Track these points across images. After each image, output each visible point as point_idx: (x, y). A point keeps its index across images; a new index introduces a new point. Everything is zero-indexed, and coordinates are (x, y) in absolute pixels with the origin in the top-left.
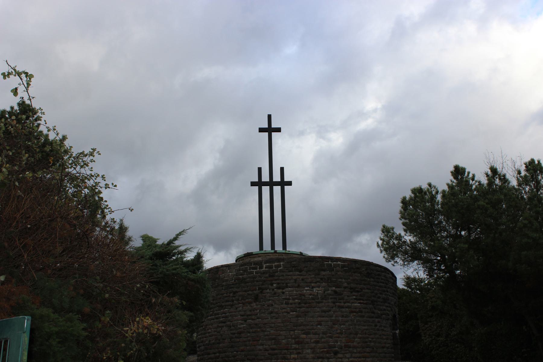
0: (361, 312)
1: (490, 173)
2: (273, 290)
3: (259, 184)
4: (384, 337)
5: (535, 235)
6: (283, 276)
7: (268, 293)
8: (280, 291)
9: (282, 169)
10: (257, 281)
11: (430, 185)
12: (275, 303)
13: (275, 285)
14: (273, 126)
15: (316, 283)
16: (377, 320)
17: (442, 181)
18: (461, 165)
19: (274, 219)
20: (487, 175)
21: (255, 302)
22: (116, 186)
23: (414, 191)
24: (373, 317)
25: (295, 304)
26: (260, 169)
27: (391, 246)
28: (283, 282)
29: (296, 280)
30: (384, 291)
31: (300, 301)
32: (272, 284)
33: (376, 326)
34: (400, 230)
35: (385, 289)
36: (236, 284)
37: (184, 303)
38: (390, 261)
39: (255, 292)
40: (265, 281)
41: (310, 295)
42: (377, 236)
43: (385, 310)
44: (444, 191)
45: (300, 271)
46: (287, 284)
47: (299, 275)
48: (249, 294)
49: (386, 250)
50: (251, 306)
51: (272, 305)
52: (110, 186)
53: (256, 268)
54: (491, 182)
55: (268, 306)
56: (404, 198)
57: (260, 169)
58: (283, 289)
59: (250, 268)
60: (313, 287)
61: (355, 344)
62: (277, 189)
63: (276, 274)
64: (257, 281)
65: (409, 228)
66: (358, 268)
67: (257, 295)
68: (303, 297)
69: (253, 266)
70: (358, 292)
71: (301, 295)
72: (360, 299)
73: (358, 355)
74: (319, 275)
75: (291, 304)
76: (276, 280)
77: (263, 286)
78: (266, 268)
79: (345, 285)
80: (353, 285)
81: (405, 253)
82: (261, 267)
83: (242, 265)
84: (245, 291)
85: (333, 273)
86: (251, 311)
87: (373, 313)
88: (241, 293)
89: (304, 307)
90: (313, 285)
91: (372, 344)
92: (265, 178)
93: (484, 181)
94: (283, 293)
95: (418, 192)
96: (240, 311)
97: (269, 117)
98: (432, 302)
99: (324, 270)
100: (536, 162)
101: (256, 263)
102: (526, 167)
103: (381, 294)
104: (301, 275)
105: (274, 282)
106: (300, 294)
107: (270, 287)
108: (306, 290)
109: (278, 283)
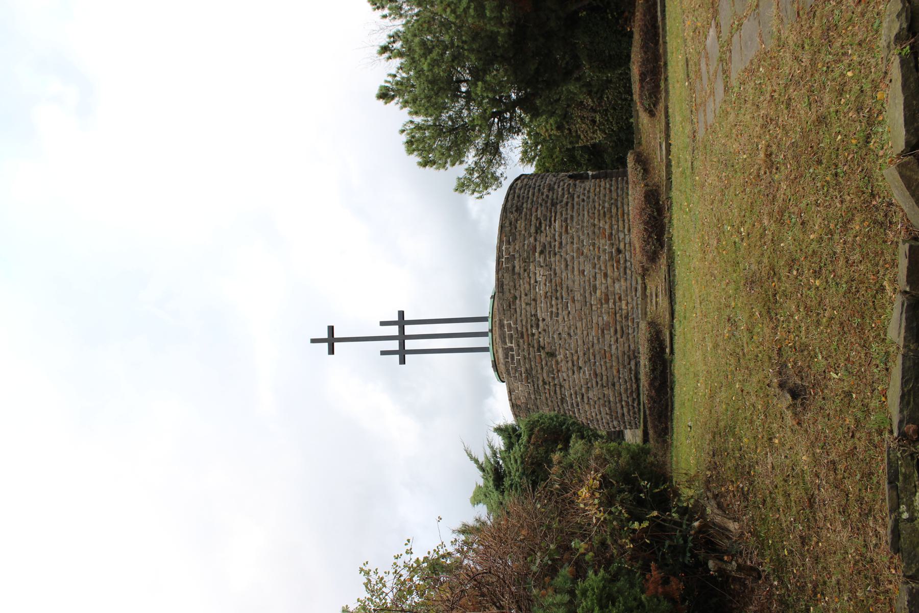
1: (387, 55)
3: (402, 354)
4: (598, 190)
8: (540, 323)
9: (383, 324)
11: (403, 131)
16: (576, 199)
17: (397, 115)
18: (376, 91)
20: (390, 58)
22: (409, 541)
24: (573, 204)
26: (383, 353)
27: (483, 179)
29: (527, 304)
30: (539, 190)
32: (533, 335)
33: (583, 200)
34: (459, 171)
43: (563, 189)
44: (410, 113)
45: (515, 298)
52: (408, 547)
53: (513, 356)
56: (420, 164)
57: (383, 353)
60: (536, 282)
61: (607, 227)
63: (519, 329)
65: (458, 157)
66: (511, 224)
67: (547, 353)
68: (549, 294)
70: (540, 223)
72: (550, 221)
73: (621, 223)
74: (519, 274)
76: (527, 330)
77: (536, 345)
79: (532, 240)
80: (533, 230)
81: (490, 162)
82: (511, 349)
83: (509, 374)
84: (542, 368)
85: (517, 255)
87: (567, 204)
88: (545, 375)
91: (606, 205)
94: (544, 320)
97: (314, 341)
99: (514, 267)
102: (378, 8)
107: (536, 337)
109: (532, 326)
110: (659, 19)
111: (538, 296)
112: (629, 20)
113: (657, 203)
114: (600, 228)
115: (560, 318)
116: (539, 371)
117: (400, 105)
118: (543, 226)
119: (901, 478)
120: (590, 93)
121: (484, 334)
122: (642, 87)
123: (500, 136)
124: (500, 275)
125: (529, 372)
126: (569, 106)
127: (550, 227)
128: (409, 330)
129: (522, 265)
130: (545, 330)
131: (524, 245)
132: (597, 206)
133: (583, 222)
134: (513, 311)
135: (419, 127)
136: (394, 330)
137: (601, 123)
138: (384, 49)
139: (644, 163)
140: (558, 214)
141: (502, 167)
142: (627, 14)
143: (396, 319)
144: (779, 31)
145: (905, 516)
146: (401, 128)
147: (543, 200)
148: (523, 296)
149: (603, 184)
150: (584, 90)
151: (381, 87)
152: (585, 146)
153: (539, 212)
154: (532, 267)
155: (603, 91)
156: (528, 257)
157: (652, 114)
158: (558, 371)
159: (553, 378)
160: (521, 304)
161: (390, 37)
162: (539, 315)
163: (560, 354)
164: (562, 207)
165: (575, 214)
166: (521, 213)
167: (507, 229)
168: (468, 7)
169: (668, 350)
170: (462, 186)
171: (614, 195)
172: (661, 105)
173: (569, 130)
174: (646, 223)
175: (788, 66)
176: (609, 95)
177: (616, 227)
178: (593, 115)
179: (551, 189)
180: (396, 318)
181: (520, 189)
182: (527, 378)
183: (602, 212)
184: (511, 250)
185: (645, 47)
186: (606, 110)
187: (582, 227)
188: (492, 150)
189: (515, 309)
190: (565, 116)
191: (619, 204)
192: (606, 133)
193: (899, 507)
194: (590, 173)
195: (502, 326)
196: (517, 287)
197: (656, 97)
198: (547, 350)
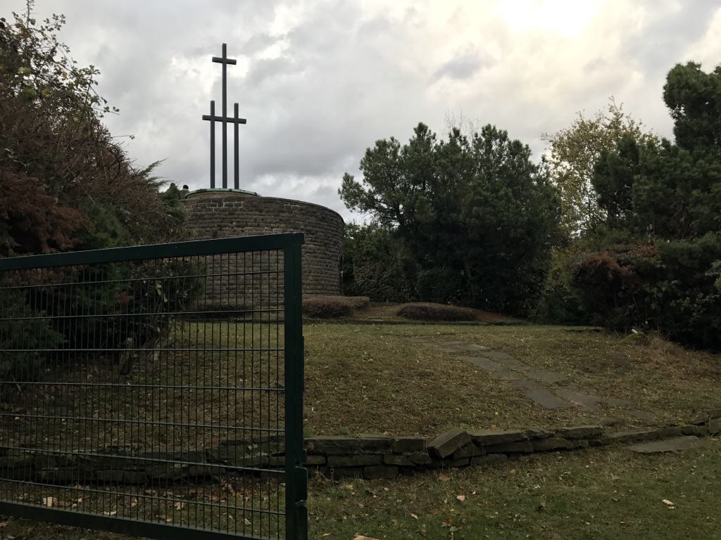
0: (315, 253)
1: (453, 134)
2: (233, 228)
3: (212, 118)
4: (333, 276)
5: (487, 194)
6: (243, 214)
8: (241, 229)
9: (236, 106)
11: (392, 139)
15: (275, 223)
16: (328, 261)
17: (405, 138)
18: (425, 123)
19: (225, 157)
20: (450, 136)
22: (118, 110)
23: (378, 143)
24: (325, 258)
26: (213, 104)
27: (351, 193)
29: (256, 219)
30: (335, 235)
32: (232, 223)
33: (327, 266)
34: (359, 178)
35: (336, 233)
37: (357, 231)
38: (349, 208)
39: (214, 229)
40: (224, 219)
42: (338, 183)
43: (335, 252)
44: (405, 146)
45: (261, 212)
46: (247, 222)
47: (258, 215)
48: (207, 231)
49: (346, 198)
52: (111, 109)
53: (215, 206)
54: (453, 142)
56: (368, 150)
57: (213, 104)
60: (272, 228)
61: (308, 281)
62: (230, 126)
65: (370, 179)
66: (314, 212)
67: (216, 232)
70: (313, 234)
72: (315, 241)
73: (310, 291)
74: (278, 216)
76: (235, 218)
77: (223, 224)
79: (303, 227)
80: (309, 228)
81: (362, 201)
82: (221, 205)
83: (200, 202)
84: (203, 227)
85: (292, 215)
87: (325, 254)
91: (323, 282)
92: (219, 113)
93: (447, 141)
94: (243, 231)
95: (382, 145)
97: (224, 46)
98: (367, 248)
99: (284, 212)
100: (492, 128)
101: (215, 201)
102: (483, 131)
103: (333, 237)
107: (229, 224)
108: (266, 230)
109: (238, 222)
110: (461, 322)
112: (455, 303)
113: (341, 314)
114: (308, 276)
116: (201, 225)
117: (413, 139)
118: (311, 236)
119: (276, 444)
120: (392, 276)
121: (225, 184)
122: (417, 308)
123: (380, 209)
124: (278, 201)
125: (201, 217)
126: (384, 261)
127: (311, 241)
129: (285, 219)
130: (234, 231)
131: (299, 221)
132: (323, 275)
133: (313, 264)
134: (251, 209)
135: (394, 153)
136: (231, 115)
137: (369, 283)
138: (457, 132)
139: (362, 308)
140: (318, 247)
141: (359, 209)
142: (458, 301)
143: (240, 117)
144: (503, 380)
145: (250, 447)
146: (395, 138)
147: (329, 237)
148: (262, 217)
149: (337, 280)
150: (395, 272)
151: (427, 127)
152: (353, 271)
153: (321, 234)
154: (282, 225)
155: (393, 286)
156: (290, 223)
157: (399, 314)
160: (256, 215)
161: (465, 138)
164: (323, 250)
165: (318, 259)
166: (321, 220)
167: (310, 210)
168: (481, 195)
169: (238, 319)
170: (348, 179)
171: (329, 288)
172: (405, 320)
173: (366, 260)
174: (329, 306)
175: (486, 386)
176: (390, 289)
177: (308, 288)
178: (376, 278)
179: (336, 243)
181: (336, 221)
182: (196, 215)
183: (318, 278)
184: (296, 211)
185: (443, 311)
186: (378, 287)
187: (309, 264)
188: (369, 203)
189: (252, 211)
190: (376, 258)
191: (323, 291)
192: (361, 286)
193: (255, 443)
194: (342, 272)
195: (239, 199)
196: (269, 213)
197: (411, 317)
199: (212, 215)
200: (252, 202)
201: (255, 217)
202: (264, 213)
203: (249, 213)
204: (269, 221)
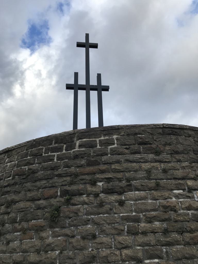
2: (97, 195)
6: (118, 162)
7: (84, 203)
8: (113, 198)
9: (99, 76)
10: (60, 176)
12: (103, 231)
13: (100, 184)
14: (90, 42)
21: (51, 227)
25: (154, 232)
26: (76, 75)
28: (120, 175)
29: (149, 172)
31: (165, 225)
32: (94, 183)
36: (15, 184)
39: (53, 201)
40: (76, 175)
41: (189, 208)
45: (157, 153)
46: (128, 180)
47: (156, 161)
48: (39, 208)
50: (42, 239)
51: (94, 237)
55: (83, 238)
57: (76, 75)
58: (120, 193)
59: (47, 151)
63: (104, 158)
64: (60, 176)
67: (58, 209)
68: (172, 215)
69: (53, 145)
71: (166, 208)
75: (144, 233)
76: (102, 172)
77: (74, 188)
78: (80, 146)
82: (71, 146)
84: (33, 200)
86: (38, 252)
88: (22, 205)
89: (178, 243)
90: (190, 183)
94: (121, 203)
96: (14, 251)
104: (160, 162)
105: (98, 176)
106: (165, 207)
107: (89, 188)
108: (177, 196)
109: (109, 180)
111: (166, 194)
115: (125, 239)
116: (29, 195)
124: (190, 132)
128: (94, 94)
130: (101, 205)
158: (24, 231)
159: (14, 221)
160: (148, 163)
162: (131, 194)
163: (55, 235)
180: (104, 83)
189: (139, 153)
196: (178, 157)
198: (64, 209)
199: (52, 169)
200: (136, 134)
201: (146, 166)
202: (164, 156)
203: (131, 157)
204: (180, 173)
